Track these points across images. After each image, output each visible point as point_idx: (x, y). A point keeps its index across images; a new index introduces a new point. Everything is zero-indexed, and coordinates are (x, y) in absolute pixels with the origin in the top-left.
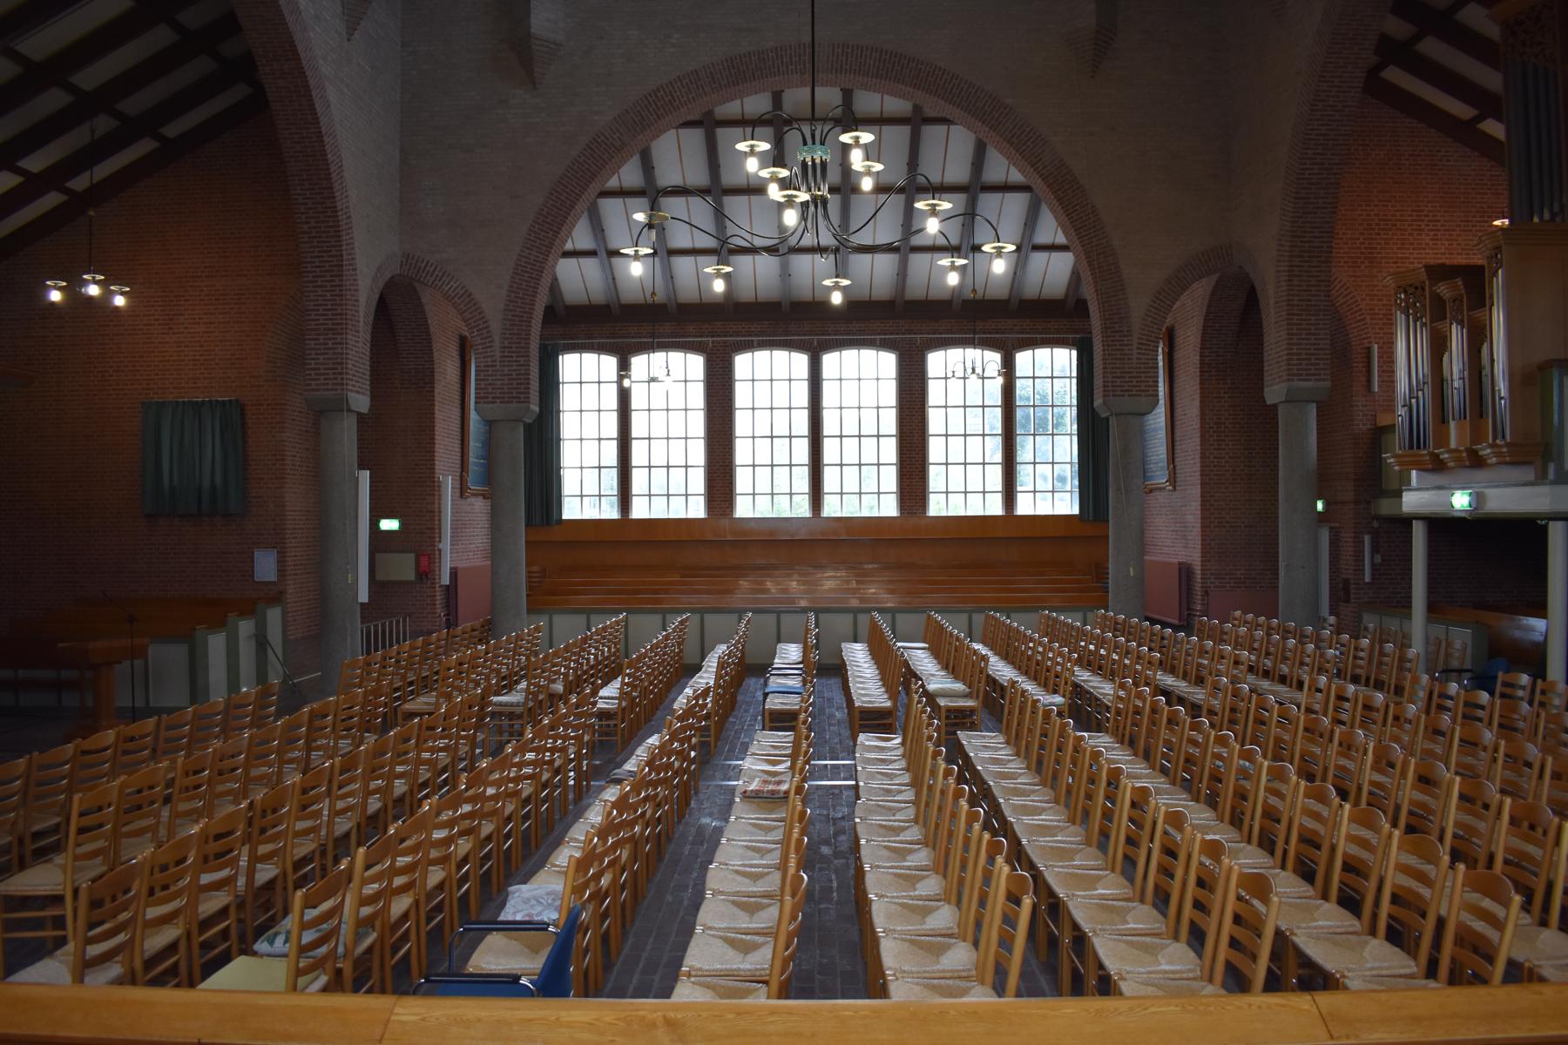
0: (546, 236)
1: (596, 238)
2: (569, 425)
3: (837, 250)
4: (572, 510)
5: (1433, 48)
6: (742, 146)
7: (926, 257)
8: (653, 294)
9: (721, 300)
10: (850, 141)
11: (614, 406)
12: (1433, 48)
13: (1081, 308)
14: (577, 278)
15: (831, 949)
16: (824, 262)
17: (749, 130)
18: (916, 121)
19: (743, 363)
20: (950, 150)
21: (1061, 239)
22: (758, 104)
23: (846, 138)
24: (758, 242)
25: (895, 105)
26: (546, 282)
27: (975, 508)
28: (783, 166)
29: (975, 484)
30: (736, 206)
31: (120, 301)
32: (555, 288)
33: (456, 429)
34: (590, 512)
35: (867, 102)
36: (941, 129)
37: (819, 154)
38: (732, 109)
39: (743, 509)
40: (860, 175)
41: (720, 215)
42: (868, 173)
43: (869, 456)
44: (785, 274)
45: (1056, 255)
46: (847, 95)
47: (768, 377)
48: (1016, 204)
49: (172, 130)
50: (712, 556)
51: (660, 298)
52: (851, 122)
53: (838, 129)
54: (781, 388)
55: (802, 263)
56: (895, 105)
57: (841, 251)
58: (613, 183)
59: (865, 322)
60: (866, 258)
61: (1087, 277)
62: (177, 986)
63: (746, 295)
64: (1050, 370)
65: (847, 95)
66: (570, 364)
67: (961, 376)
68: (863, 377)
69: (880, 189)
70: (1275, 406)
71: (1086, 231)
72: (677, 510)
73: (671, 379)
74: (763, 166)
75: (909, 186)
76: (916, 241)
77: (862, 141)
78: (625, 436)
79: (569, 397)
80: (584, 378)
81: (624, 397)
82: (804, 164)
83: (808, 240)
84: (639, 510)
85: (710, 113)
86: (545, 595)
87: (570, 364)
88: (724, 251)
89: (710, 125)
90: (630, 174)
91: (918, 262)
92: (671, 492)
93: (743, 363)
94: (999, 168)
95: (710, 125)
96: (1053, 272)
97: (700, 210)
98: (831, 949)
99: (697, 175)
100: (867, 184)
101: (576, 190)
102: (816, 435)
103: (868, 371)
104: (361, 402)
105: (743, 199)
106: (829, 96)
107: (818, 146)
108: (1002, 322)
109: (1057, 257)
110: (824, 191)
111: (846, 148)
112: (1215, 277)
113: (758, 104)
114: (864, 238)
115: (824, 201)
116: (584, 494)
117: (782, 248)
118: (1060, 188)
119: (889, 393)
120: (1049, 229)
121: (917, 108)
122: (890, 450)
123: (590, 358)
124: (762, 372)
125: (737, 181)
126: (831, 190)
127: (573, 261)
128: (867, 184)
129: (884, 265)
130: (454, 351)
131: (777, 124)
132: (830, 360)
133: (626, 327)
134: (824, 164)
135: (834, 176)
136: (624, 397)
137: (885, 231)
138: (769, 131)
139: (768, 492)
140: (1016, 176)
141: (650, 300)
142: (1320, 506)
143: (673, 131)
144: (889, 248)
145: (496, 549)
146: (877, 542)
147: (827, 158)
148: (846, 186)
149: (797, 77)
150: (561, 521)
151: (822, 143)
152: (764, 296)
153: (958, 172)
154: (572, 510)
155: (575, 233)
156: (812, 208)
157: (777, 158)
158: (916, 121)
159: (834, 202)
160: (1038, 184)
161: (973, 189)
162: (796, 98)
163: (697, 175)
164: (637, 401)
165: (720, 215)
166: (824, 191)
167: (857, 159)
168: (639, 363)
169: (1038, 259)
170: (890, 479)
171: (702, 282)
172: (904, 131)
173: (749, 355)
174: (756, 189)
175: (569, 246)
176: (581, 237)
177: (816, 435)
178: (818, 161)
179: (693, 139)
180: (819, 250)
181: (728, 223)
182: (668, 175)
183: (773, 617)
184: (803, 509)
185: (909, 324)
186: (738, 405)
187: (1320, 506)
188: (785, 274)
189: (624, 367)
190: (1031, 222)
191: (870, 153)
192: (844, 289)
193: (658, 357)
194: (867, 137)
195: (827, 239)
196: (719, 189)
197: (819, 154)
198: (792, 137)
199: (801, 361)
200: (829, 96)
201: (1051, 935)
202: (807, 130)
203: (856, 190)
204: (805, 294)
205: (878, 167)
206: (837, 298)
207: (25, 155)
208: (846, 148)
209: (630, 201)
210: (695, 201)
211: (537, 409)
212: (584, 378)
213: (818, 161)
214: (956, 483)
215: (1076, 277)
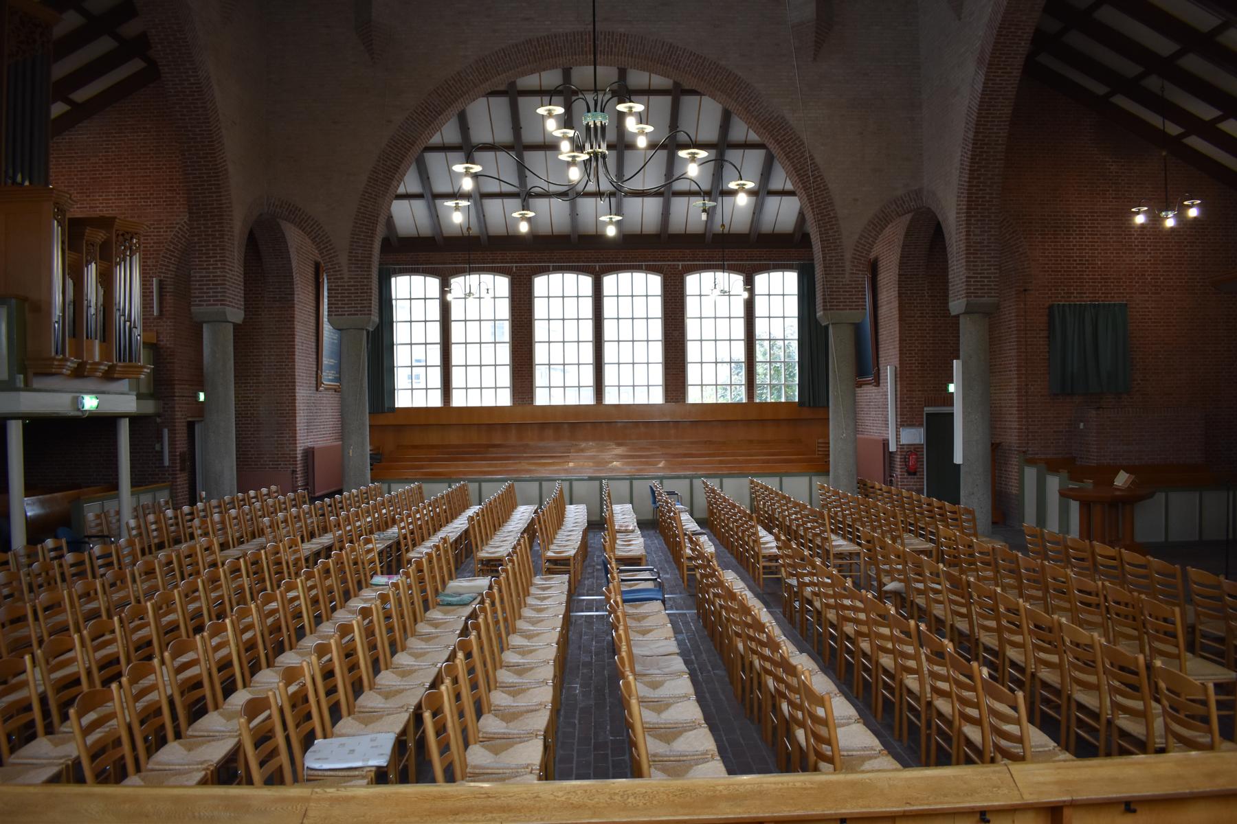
0: (382, 184)
1: (424, 187)
2: (401, 333)
3: (612, 194)
4: (403, 400)
5: (1076, 39)
6: (542, 111)
7: (684, 200)
8: (469, 228)
9: (457, 233)
10: (626, 110)
11: (742, 313)
12: (1076, 39)
13: (806, 238)
14: (408, 216)
15: (593, 734)
16: (603, 203)
17: (546, 99)
18: (677, 93)
19: (693, 282)
20: (703, 116)
21: (789, 186)
22: (551, 78)
23: (622, 107)
24: (553, 189)
25: (658, 81)
26: (382, 220)
27: (572, 399)
28: (572, 128)
29: (488, 381)
30: (534, 160)
31: (1193, 213)
32: (390, 220)
33: (318, 337)
34: (419, 401)
35: (638, 78)
36: (694, 100)
37: (599, 119)
38: (531, 81)
39: (541, 398)
40: (635, 135)
41: (522, 169)
42: (642, 132)
43: (488, 359)
44: (574, 213)
45: (785, 199)
46: (622, 73)
47: (560, 294)
48: (755, 158)
49: (81, 96)
50: (519, 433)
51: (475, 231)
52: (625, 94)
53: (615, 99)
54: (640, 302)
55: (588, 206)
56: (658, 81)
57: (617, 195)
58: (436, 139)
59: (633, 251)
60: (638, 201)
61: (809, 216)
62: (239, 784)
63: (544, 229)
64: (780, 291)
65: (622, 73)
66: (402, 286)
67: (712, 294)
68: (635, 293)
69: (652, 146)
70: (957, 316)
71: (810, 184)
72: (488, 401)
73: (483, 296)
74: (559, 128)
75: (669, 145)
76: (680, 186)
77: (555, 113)
78: (448, 342)
79: (400, 311)
80: (412, 294)
81: (445, 308)
82: (588, 127)
83: (592, 187)
84: (458, 400)
85: (513, 84)
86: (384, 465)
87: (402, 286)
88: (525, 196)
89: (513, 94)
90: (449, 133)
91: (679, 204)
92: (484, 385)
93: (693, 282)
94: (740, 131)
95: (513, 94)
96: (783, 213)
97: (506, 161)
98: (593, 734)
99: (504, 134)
100: (642, 142)
101: (405, 150)
102: (601, 341)
103: (639, 289)
104: (236, 314)
105: (541, 154)
106: (607, 74)
107: (599, 112)
108: (747, 252)
109: (787, 200)
110: (604, 149)
111: (621, 116)
112: (909, 217)
113: (551, 78)
114: (636, 184)
115: (604, 156)
116: (414, 389)
117: (571, 194)
118: (781, 146)
119: (504, 309)
120: (780, 180)
121: (676, 84)
122: (504, 354)
123: (418, 280)
124: (556, 290)
125: (537, 139)
126: (609, 147)
127: (405, 202)
128: (642, 142)
129: (651, 207)
130: (310, 271)
131: (566, 94)
132: (609, 281)
133: (446, 255)
134: (603, 127)
135: (611, 136)
136: (445, 308)
137: (651, 179)
138: (561, 99)
139: (561, 384)
140: (753, 137)
141: (466, 233)
142: (202, 397)
143: (483, 100)
144: (657, 194)
145: (343, 431)
146: (695, 423)
147: (606, 122)
148: (623, 144)
149: (590, 55)
150: (393, 409)
151: (602, 111)
152: (557, 230)
153: (709, 132)
154: (403, 400)
155: (406, 178)
156: (594, 164)
157: (567, 121)
158: (677, 93)
159: (612, 157)
160: (417, 150)
161: (721, 147)
162: (582, 74)
163: (504, 134)
164: (456, 313)
165: (522, 169)
166: (604, 149)
167: (631, 124)
168: (457, 283)
169: (772, 203)
170: (505, 376)
171: (509, 223)
172: (666, 101)
173: (766, 275)
174: (551, 146)
175: (401, 190)
176: (411, 183)
177: (601, 341)
178: (599, 124)
179: (500, 105)
180: (599, 194)
181: (528, 173)
182: (480, 134)
183: (537, 484)
184: (588, 398)
185: (671, 254)
186: (536, 317)
187: (202, 397)
188: (574, 213)
189: (445, 287)
190: (766, 175)
191: (641, 118)
192: (618, 223)
193: (473, 279)
194: (638, 107)
195: (605, 186)
196: (523, 145)
197: (599, 119)
198: (579, 105)
199: (586, 282)
200: (607, 74)
201: (910, 722)
202: (590, 98)
203: (631, 146)
204: (591, 230)
205: (649, 129)
206: (611, 231)
207: (67, 112)
208: (621, 116)
209: (451, 155)
210: (502, 155)
211: (377, 320)
212: (412, 294)
213: (599, 124)
214: (474, 381)
215: (801, 217)
